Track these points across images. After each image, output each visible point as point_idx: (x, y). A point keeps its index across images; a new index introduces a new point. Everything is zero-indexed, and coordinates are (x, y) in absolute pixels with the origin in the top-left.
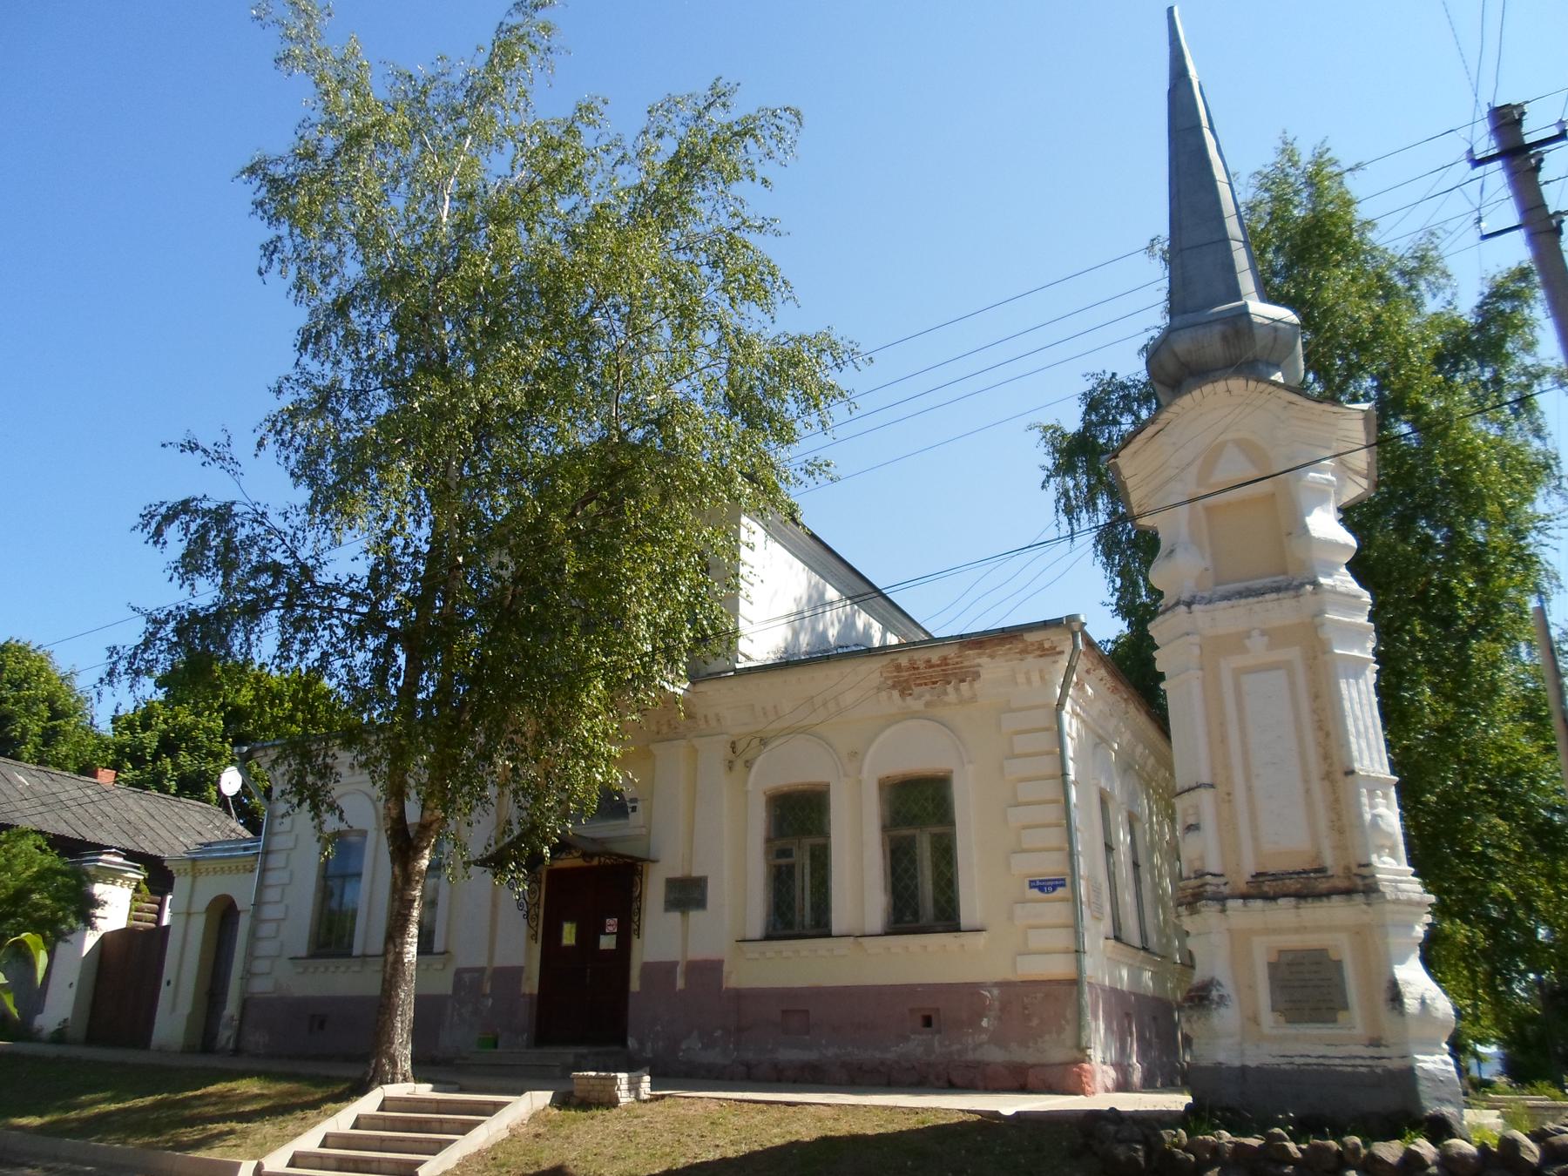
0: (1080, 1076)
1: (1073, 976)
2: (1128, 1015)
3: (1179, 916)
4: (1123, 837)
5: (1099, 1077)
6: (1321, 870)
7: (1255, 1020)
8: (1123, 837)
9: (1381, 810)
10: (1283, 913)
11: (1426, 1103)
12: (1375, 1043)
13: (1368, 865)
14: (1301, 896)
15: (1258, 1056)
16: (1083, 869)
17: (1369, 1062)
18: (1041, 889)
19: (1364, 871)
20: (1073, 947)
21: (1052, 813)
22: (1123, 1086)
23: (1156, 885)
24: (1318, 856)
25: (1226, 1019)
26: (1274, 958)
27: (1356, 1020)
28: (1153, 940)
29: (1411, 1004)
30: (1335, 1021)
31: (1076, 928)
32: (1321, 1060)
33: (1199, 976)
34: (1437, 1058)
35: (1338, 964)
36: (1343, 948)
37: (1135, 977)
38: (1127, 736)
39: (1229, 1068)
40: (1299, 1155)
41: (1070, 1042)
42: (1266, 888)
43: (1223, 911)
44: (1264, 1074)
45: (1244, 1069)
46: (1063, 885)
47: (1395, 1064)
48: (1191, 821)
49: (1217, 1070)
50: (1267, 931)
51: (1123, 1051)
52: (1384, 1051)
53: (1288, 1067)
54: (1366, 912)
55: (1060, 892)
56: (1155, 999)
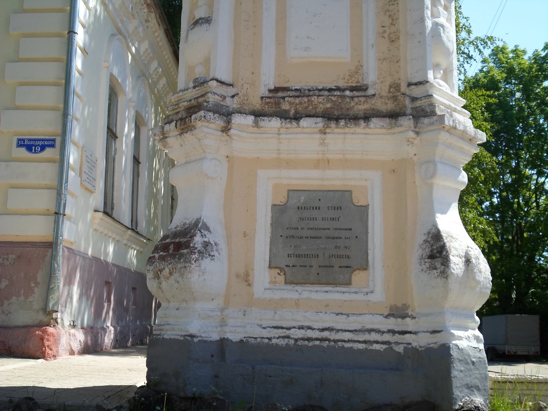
0: (42, 339)
1: (50, 239)
2: (108, 283)
3: (164, 137)
4: (127, 130)
5: (64, 340)
6: (360, 88)
7: (246, 278)
8: (127, 130)
9: (442, 20)
10: (305, 138)
11: (457, 392)
12: (399, 312)
13: (424, 82)
14: (331, 117)
15: (244, 326)
16: (76, 132)
17: (387, 337)
18: (29, 148)
19: (416, 91)
20: (54, 210)
21: (53, 72)
22: (92, 348)
23: (152, 184)
24: (358, 69)
25: (209, 275)
26: (281, 199)
27: (375, 286)
28: (142, 226)
29: (456, 264)
30: (348, 283)
31: (59, 190)
32: (326, 334)
33: (182, 217)
34: (470, 333)
35: (364, 210)
36: (372, 191)
37: (120, 252)
38: (145, 45)
39: (204, 342)
40: (129, 261)
41: (37, 305)
42: (285, 106)
43: (226, 130)
44: (248, 352)
45: (223, 342)
46: (53, 146)
47: (421, 341)
48: (200, 13)
49: (188, 342)
50: (280, 163)
51: (98, 314)
52: (409, 324)
53: (282, 342)
54: (409, 142)
55: (48, 153)
56: (136, 273)
